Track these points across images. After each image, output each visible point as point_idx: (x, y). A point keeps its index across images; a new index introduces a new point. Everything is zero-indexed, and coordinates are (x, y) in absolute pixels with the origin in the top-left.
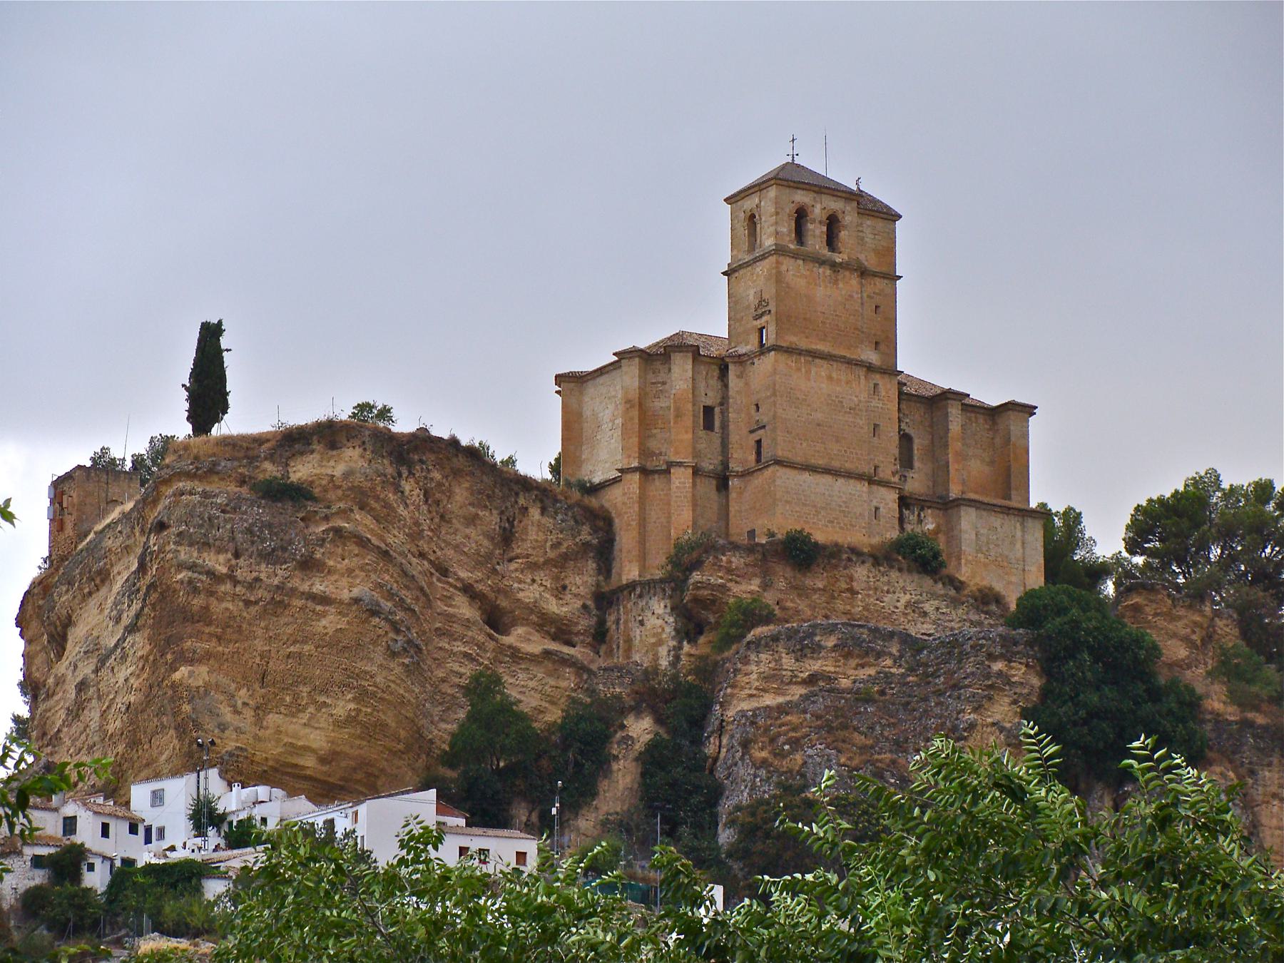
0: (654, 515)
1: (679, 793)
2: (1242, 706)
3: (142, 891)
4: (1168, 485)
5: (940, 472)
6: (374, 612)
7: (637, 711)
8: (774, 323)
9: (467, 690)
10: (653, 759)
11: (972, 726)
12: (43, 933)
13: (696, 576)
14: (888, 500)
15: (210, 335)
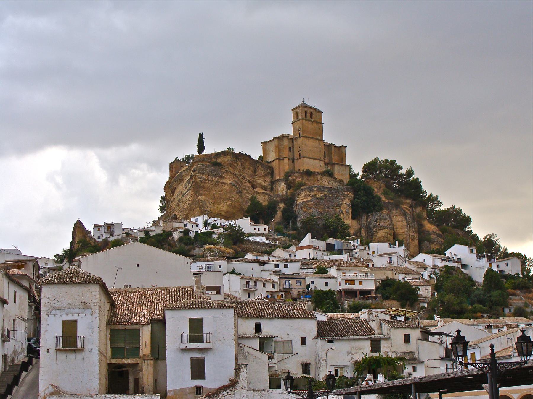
0: (281, 167)
1: (289, 217)
2: (388, 199)
3: (201, 237)
4: (369, 160)
5: (331, 158)
6: (234, 186)
7: (281, 202)
8: (301, 133)
9: (250, 200)
10: (284, 211)
11: (342, 204)
12: (183, 245)
13: (290, 178)
14: (323, 163)
15: (201, 136)
